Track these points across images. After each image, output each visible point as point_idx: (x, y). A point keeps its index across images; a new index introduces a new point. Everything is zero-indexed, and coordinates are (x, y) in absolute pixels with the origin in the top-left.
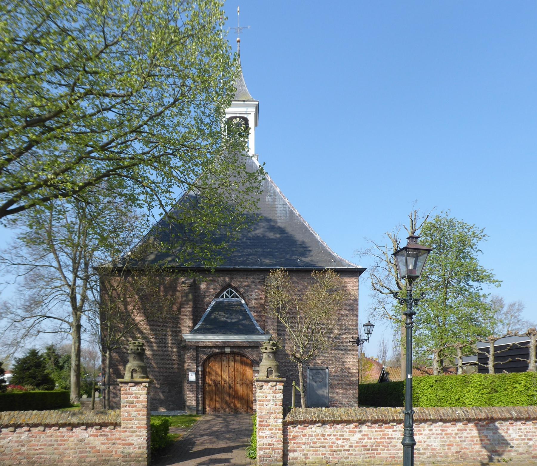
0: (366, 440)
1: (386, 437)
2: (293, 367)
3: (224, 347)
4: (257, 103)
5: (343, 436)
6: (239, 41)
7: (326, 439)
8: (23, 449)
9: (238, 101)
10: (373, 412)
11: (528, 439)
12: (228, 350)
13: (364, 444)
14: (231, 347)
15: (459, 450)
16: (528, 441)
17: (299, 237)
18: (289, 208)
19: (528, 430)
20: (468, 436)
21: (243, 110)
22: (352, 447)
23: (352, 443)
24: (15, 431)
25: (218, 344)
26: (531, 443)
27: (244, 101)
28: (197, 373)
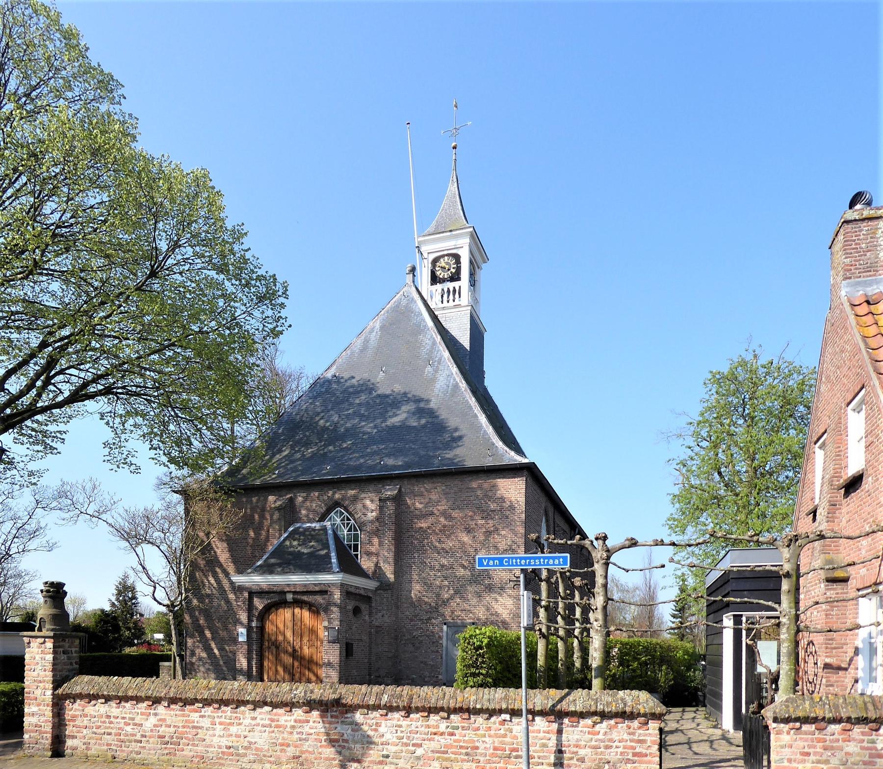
3: (284, 593)
6: (455, 148)
11: (414, 745)
18: (455, 379)
25: (275, 589)
26: (419, 752)
27: (451, 231)
28: (249, 629)
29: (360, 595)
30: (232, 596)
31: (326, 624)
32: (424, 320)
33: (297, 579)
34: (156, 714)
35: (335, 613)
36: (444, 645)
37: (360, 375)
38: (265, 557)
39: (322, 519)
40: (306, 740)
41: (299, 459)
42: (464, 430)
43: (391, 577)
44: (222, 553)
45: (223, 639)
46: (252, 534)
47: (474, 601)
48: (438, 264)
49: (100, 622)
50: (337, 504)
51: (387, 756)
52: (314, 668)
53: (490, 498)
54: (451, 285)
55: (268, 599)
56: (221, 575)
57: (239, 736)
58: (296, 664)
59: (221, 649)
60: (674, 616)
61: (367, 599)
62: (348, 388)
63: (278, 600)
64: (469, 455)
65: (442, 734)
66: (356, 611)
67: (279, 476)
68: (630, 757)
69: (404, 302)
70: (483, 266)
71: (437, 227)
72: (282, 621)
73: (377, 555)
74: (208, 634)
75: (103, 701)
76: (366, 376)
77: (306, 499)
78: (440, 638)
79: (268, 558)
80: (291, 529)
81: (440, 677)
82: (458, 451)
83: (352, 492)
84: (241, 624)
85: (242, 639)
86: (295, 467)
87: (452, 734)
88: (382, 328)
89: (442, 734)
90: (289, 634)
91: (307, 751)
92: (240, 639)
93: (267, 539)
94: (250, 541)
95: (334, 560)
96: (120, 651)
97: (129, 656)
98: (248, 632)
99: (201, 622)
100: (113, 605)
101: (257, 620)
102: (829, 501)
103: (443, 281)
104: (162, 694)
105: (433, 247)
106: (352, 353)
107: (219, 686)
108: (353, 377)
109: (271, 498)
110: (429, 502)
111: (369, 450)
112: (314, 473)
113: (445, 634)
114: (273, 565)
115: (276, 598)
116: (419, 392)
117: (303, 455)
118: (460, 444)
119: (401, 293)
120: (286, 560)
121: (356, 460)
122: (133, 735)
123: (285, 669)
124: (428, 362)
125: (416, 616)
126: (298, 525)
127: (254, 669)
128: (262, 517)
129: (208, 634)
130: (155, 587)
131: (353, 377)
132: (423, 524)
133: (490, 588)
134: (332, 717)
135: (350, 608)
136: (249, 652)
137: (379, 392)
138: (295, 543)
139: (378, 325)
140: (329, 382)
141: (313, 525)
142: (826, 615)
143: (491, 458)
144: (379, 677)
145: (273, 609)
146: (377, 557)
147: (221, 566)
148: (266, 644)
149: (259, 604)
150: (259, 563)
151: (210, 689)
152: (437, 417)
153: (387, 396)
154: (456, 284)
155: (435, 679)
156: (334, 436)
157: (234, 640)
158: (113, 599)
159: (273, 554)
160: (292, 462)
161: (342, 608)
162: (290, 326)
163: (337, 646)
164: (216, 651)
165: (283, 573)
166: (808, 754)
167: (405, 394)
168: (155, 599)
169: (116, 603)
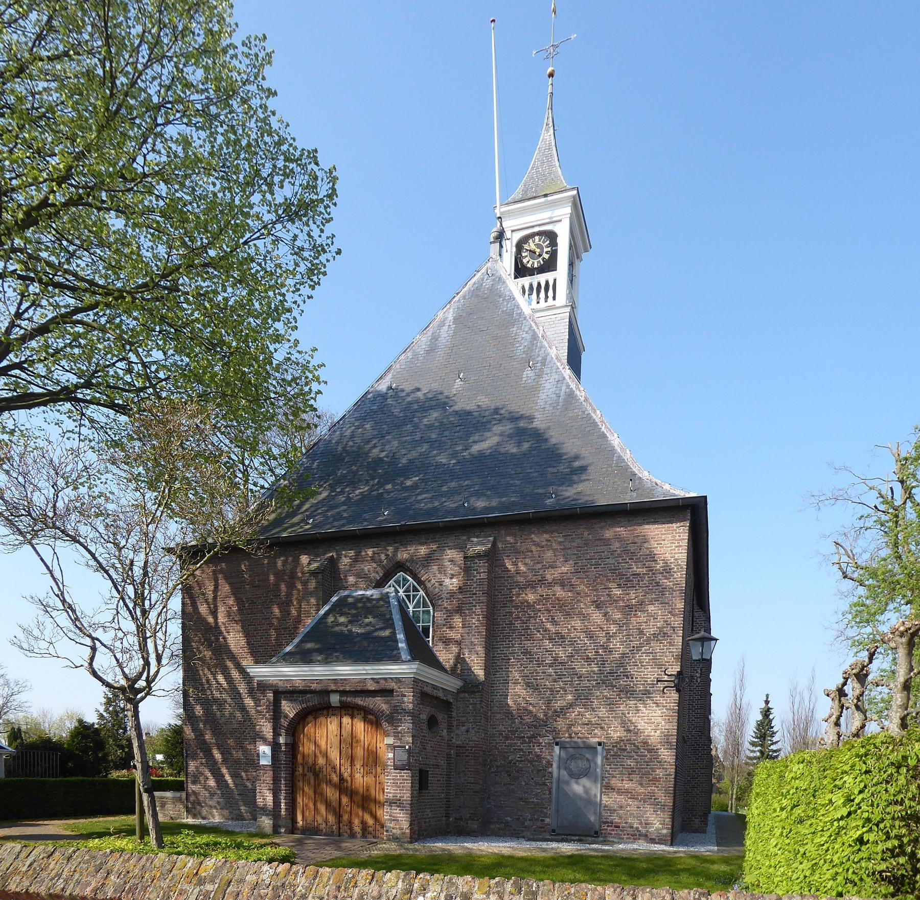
2: (524, 742)
3: (326, 693)
4: (575, 192)
6: (551, 75)
9: (535, 198)
17: (571, 446)
18: (568, 386)
21: (544, 216)
25: (314, 686)
27: (546, 196)
28: (275, 747)
29: (437, 698)
30: (249, 702)
31: (390, 740)
32: (518, 307)
33: (346, 671)
35: (406, 726)
36: (555, 774)
37: (428, 386)
38: (296, 641)
39: (380, 584)
41: (344, 504)
42: (587, 455)
43: (479, 672)
44: (235, 640)
45: (237, 761)
46: (276, 611)
47: (603, 712)
48: (526, 247)
49: (76, 736)
50: (400, 566)
52: (372, 806)
53: (632, 555)
54: (542, 278)
55: (301, 702)
56: (235, 674)
58: (345, 800)
59: (234, 776)
60: (753, 744)
61: (446, 705)
62: (410, 403)
63: (317, 704)
64: (597, 491)
66: (432, 722)
67: (314, 526)
69: (488, 283)
70: (584, 255)
71: (525, 191)
72: (326, 736)
73: (459, 643)
74: (218, 756)
76: (436, 386)
77: (356, 560)
78: (550, 764)
79: (301, 641)
80: (334, 599)
81: (547, 820)
82: (580, 488)
83: (423, 550)
84: (265, 741)
85: (265, 761)
86: (338, 513)
88: (456, 320)
90: (334, 755)
92: (263, 762)
93: (298, 620)
94: (275, 622)
95: (402, 645)
96: (106, 776)
97: (116, 782)
98: (273, 751)
99: (207, 737)
100: (101, 716)
101: (287, 734)
103: (531, 272)
104: (88, 891)
105: (517, 224)
106: (415, 355)
107: (225, 875)
108: (418, 390)
109: (304, 559)
110: (543, 561)
111: (445, 489)
112: (366, 520)
113: (556, 759)
114: (310, 651)
115: (315, 701)
116: (516, 406)
117: (349, 499)
118: (584, 477)
119: (484, 270)
120: (327, 644)
121: (424, 501)
123: (328, 805)
124: (527, 361)
125: (513, 732)
126: (346, 593)
127: (283, 806)
128: (291, 586)
129: (218, 756)
130: (94, 649)
131: (418, 390)
132: (531, 597)
133: (628, 692)
135: (424, 717)
136: (276, 780)
137: (456, 408)
138: (342, 619)
139: (450, 316)
140: (383, 396)
141: (369, 593)
143: (634, 494)
144: (461, 819)
145: (310, 718)
146: (462, 645)
147: (233, 658)
148: (301, 769)
149: (289, 709)
150: (288, 649)
151: (201, 882)
152: (546, 440)
153: (469, 413)
154: (549, 276)
155: (539, 824)
156: (392, 471)
157: (253, 762)
158: (102, 709)
159: (307, 637)
160: (332, 508)
161: (414, 715)
162: (339, 252)
163: (406, 774)
164: (228, 778)
165: (326, 662)
167: (496, 411)
168: (94, 674)
169: (105, 714)
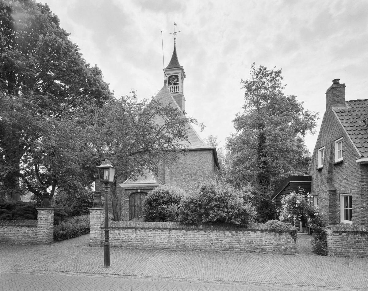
0: (138, 237)
1: (148, 236)
5: (128, 235)
7: (120, 236)
8: (5, 234)
10: (152, 224)
11: (221, 240)
12: (139, 191)
13: (137, 239)
14: (141, 189)
15: (183, 244)
16: (221, 241)
19: (221, 235)
20: (188, 237)
22: (132, 240)
23: (131, 238)
24: (2, 227)
26: (223, 242)
34: (136, 233)
40: (186, 239)
51: (212, 244)
57: (164, 239)
65: (230, 237)
68: (286, 243)
75: (117, 229)
87: (232, 237)
89: (230, 237)
91: (187, 243)
102: (329, 168)
122: (128, 239)
134: (195, 232)
142: (329, 201)
166: (337, 241)
